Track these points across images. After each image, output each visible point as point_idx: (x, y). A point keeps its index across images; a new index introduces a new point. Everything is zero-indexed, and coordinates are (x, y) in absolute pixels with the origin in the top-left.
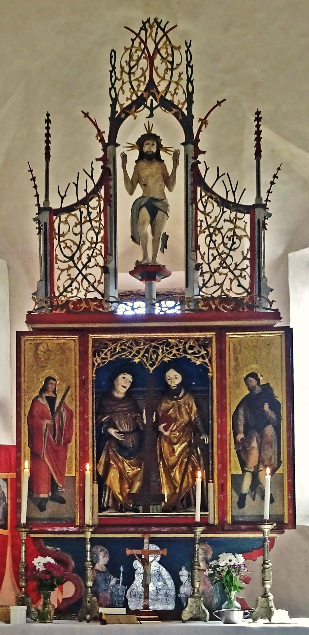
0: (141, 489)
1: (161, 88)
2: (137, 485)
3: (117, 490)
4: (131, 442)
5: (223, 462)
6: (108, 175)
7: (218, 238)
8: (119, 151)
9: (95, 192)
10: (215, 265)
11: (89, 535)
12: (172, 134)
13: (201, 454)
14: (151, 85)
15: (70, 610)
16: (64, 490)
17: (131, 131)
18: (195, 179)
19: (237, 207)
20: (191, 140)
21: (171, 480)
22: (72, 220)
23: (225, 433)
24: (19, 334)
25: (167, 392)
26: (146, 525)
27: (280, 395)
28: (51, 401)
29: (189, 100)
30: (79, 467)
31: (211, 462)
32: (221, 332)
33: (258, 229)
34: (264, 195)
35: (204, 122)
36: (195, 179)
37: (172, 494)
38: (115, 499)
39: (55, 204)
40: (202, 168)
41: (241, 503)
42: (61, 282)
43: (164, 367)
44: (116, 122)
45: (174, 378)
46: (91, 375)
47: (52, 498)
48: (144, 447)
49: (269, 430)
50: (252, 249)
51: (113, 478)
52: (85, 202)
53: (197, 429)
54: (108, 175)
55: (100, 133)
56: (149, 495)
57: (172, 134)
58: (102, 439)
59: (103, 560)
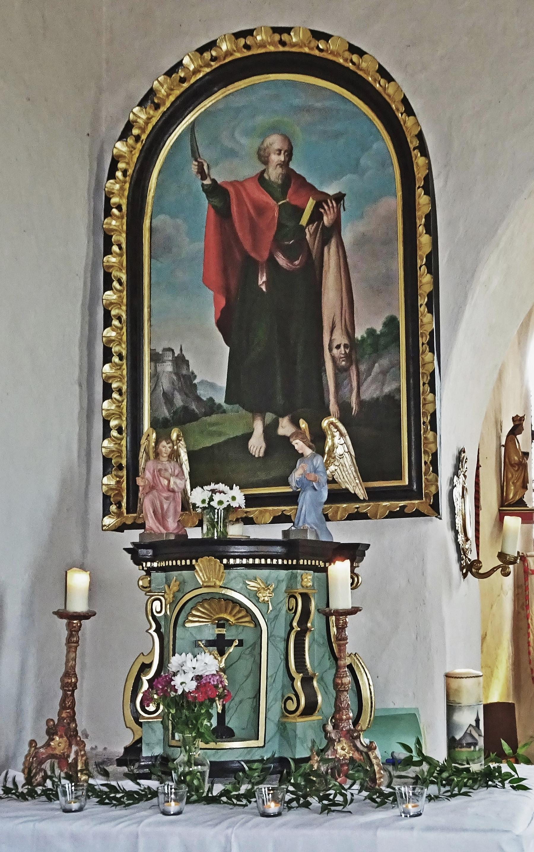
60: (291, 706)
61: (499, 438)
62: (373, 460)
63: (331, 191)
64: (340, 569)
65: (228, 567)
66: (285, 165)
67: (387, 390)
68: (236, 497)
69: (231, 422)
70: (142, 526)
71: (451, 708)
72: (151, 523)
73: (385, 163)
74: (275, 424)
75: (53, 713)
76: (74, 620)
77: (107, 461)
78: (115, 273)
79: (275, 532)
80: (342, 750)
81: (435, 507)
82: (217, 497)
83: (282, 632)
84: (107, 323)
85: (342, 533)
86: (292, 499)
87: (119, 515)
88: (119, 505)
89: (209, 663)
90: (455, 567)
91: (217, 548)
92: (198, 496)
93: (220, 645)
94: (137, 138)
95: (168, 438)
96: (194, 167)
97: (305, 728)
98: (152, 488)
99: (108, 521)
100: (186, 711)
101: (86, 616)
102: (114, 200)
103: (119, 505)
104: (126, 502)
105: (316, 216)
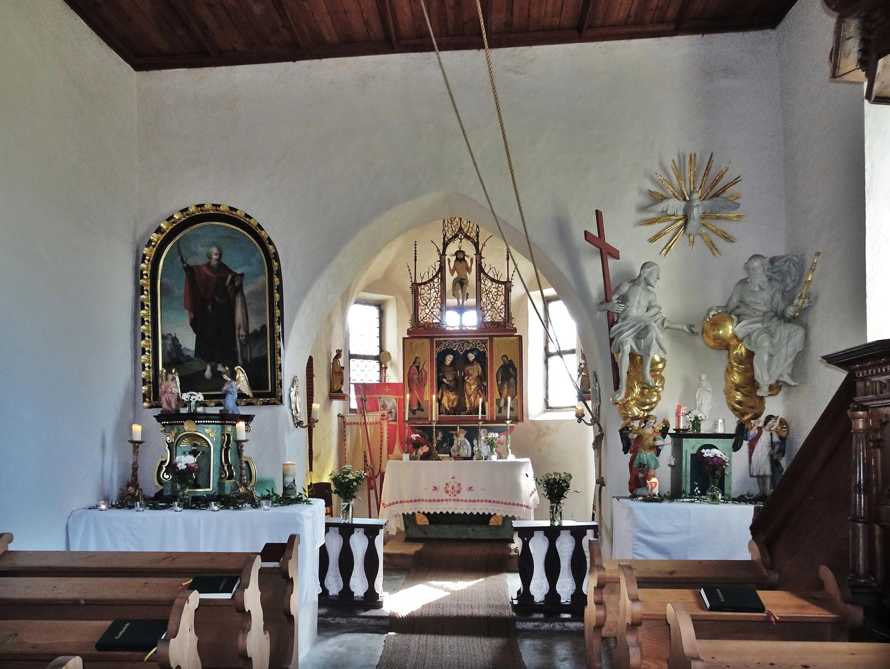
0: (457, 405)
1: (465, 230)
2: (455, 403)
3: (446, 406)
4: (452, 384)
5: (492, 393)
6: (442, 269)
7: (491, 296)
8: (447, 257)
9: (436, 275)
10: (489, 307)
11: (434, 425)
12: (469, 250)
13: (483, 390)
14: (461, 229)
15: (426, 457)
16: (423, 406)
17: (452, 248)
18: (480, 269)
19: (498, 282)
20: (478, 253)
21: (470, 401)
22: (426, 288)
23: (493, 382)
24: (404, 339)
25: (468, 362)
26: (459, 421)
27: (517, 366)
28: (418, 367)
29: (477, 235)
30: (431, 397)
31: (877, 543)
32: (491, 337)
33: (508, 291)
34: (510, 277)
35: (484, 245)
36: (480, 269)
37: (471, 407)
38: (446, 410)
39: (419, 281)
40: (483, 265)
41: (500, 411)
42: (422, 315)
43: (467, 352)
44: (445, 245)
45: (472, 357)
46: (435, 356)
47: (419, 409)
48: (458, 386)
49: (512, 380)
50: (505, 300)
51: (445, 401)
52: (432, 280)
53: (482, 378)
54: (442, 269)
55: (438, 250)
56: (459, 408)
57: (469, 250)
58: (440, 384)
59: (440, 435)
60: (223, 476)
61: (329, 360)
62: (257, 382)
63: (239, 272)
64: (241, 425)
65: (197, 424)
66: (219, 260)
67: (262, 354)
68: (200, 396)
69: (197, 366)
70: (160, 407)
71: (284, 476)
72: (165, 406)
73: (261, 262)
74: (216, 367)
75: (130, 478)
76: (136, 444)
77: (144, 380)
78: (146, 303)
79: (216, 410)
80: (242, 490)
81: (281, 401)
82: (193, 397)
83: (219, 448)
84: (143, 323)
85: (244, 411)
86: (223, 396)
87: (150, 402)
88: (150, 398)
89: (191, 460)
90: (292, 424)
91: (193, 416)
92: (185, 397)
93: (194, 453)
94: (154, 246)
95: (171, 373)
96: (179, 259)
97: (228, 483)
98: (165, 392)
99: (146, 404)
100: (183, 477)
101: (140, 442)
102: (144, 272)
103: (150, 398)
104: (154, 396)
105: (232, 282)
